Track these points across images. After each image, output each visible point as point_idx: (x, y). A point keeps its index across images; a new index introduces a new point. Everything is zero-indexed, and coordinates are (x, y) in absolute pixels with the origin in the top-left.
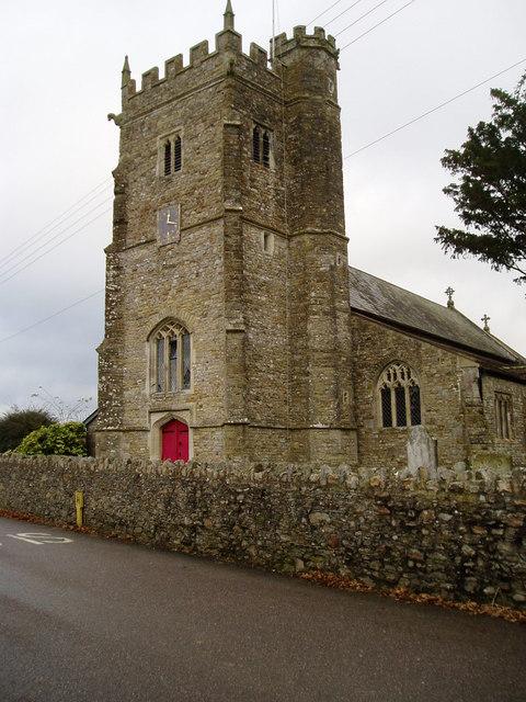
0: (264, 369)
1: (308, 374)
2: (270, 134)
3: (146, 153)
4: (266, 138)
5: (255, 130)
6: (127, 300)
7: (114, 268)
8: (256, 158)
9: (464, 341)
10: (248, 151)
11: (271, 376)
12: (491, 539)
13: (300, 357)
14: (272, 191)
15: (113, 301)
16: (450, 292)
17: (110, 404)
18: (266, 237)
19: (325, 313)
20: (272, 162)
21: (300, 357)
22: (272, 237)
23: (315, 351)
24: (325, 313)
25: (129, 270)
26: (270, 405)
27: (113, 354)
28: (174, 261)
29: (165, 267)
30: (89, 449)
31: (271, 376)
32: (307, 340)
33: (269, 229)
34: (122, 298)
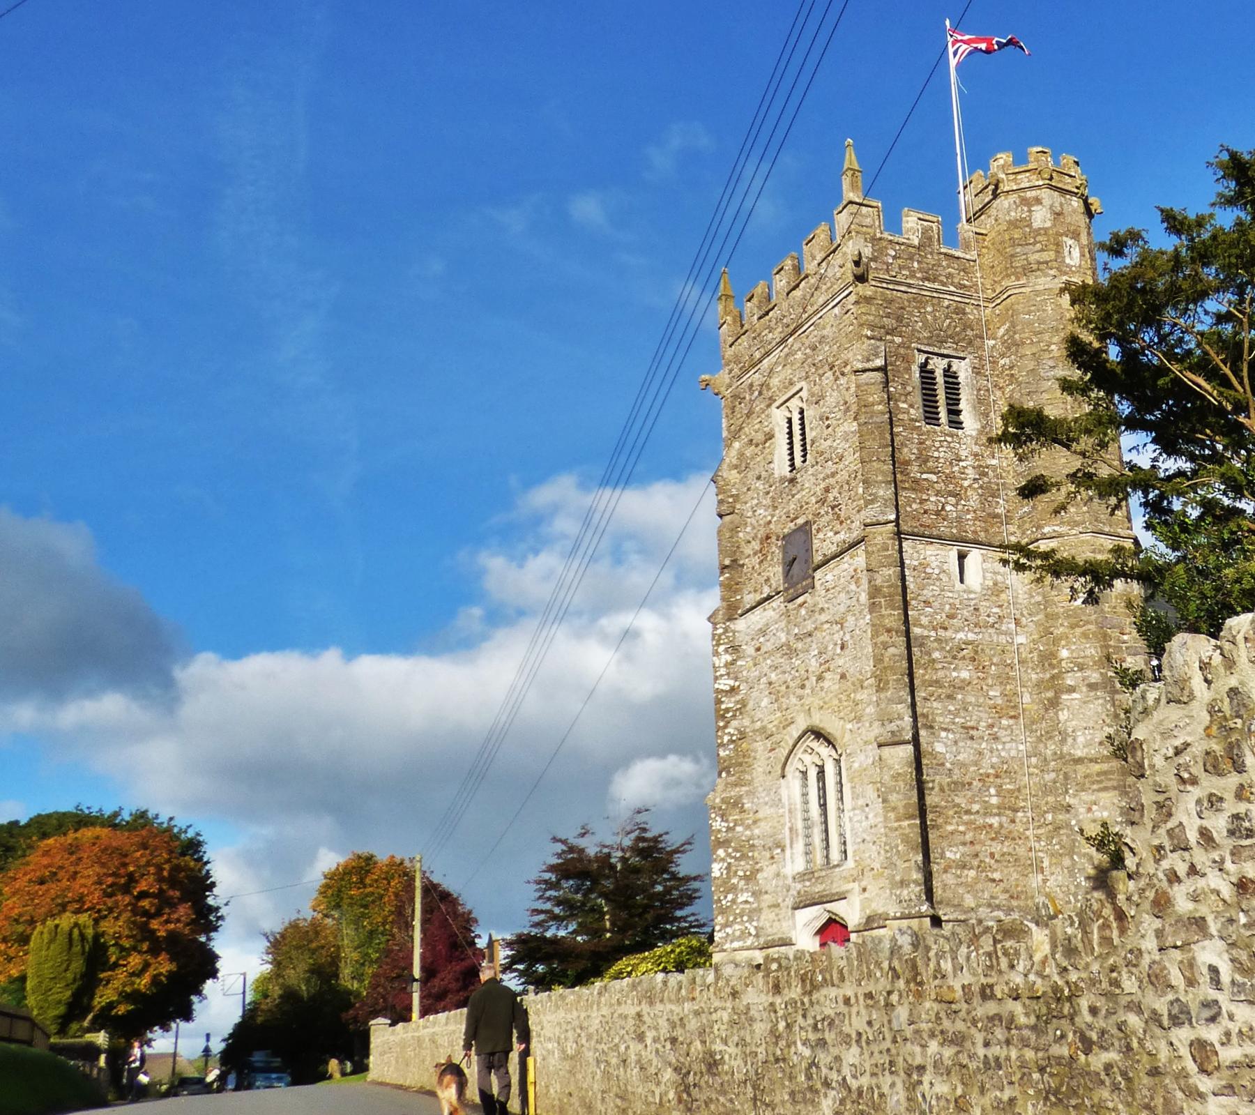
0: (976, 807)
1: (1068, 808)
2: (956, 365)
3: (760, 437)
4: (949, 374)
5: (923, 367)
6: (750, 706)
7: (726, 651)
8: (931, 416)
9: (915, 799)
10: (911, 409)
11: (994, 821)
12: (164, 966)
13: (1053, 775)
14: (970, 471)
15: (727, 710)
16: (555, 840)
17: (734, 901)
18: (962, 557)
19: (1092, 687)
20: (967, 417)
21: (1053, 775)
22: (975, 557)
23: (1079, 761)
24: (1092, 687)
25: (750, 650)
26: (996, 876)
27: (735, 804)
28: (810, 626)
29: (798, 638)
30: (849, 999)
31: (994, 821)
32: (1063, 741)
33: (963, 542)
34: (744, 703)
